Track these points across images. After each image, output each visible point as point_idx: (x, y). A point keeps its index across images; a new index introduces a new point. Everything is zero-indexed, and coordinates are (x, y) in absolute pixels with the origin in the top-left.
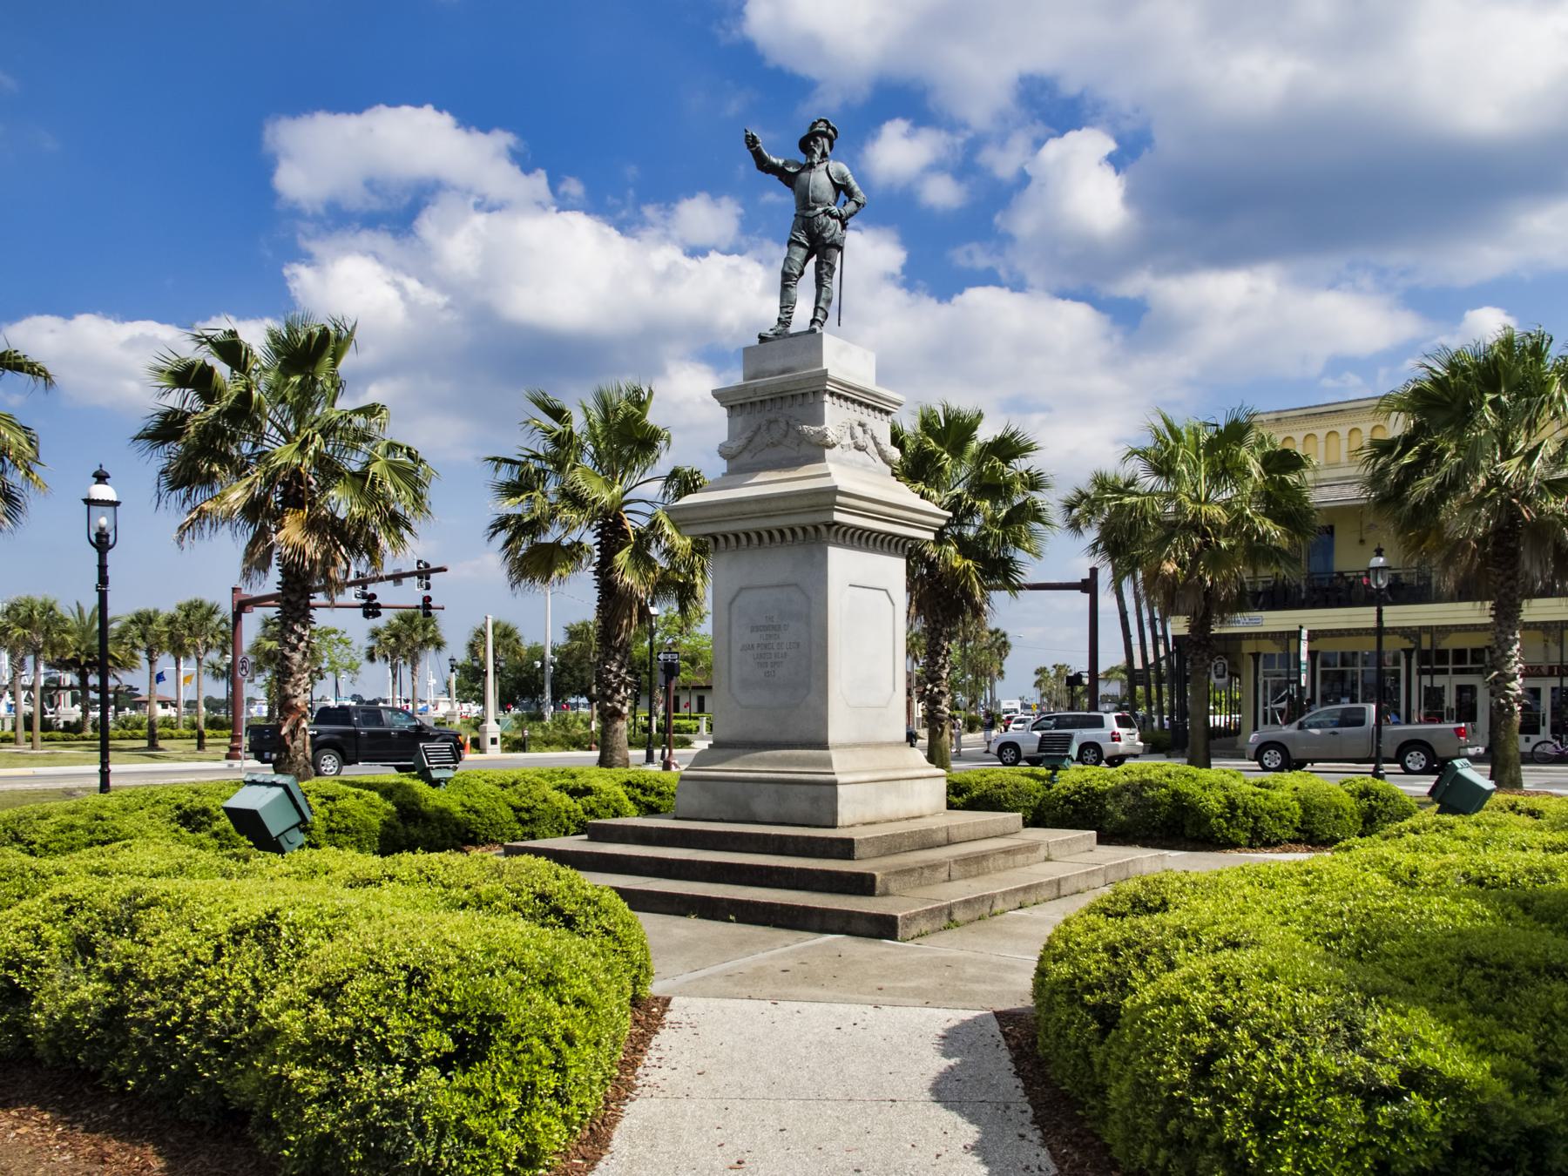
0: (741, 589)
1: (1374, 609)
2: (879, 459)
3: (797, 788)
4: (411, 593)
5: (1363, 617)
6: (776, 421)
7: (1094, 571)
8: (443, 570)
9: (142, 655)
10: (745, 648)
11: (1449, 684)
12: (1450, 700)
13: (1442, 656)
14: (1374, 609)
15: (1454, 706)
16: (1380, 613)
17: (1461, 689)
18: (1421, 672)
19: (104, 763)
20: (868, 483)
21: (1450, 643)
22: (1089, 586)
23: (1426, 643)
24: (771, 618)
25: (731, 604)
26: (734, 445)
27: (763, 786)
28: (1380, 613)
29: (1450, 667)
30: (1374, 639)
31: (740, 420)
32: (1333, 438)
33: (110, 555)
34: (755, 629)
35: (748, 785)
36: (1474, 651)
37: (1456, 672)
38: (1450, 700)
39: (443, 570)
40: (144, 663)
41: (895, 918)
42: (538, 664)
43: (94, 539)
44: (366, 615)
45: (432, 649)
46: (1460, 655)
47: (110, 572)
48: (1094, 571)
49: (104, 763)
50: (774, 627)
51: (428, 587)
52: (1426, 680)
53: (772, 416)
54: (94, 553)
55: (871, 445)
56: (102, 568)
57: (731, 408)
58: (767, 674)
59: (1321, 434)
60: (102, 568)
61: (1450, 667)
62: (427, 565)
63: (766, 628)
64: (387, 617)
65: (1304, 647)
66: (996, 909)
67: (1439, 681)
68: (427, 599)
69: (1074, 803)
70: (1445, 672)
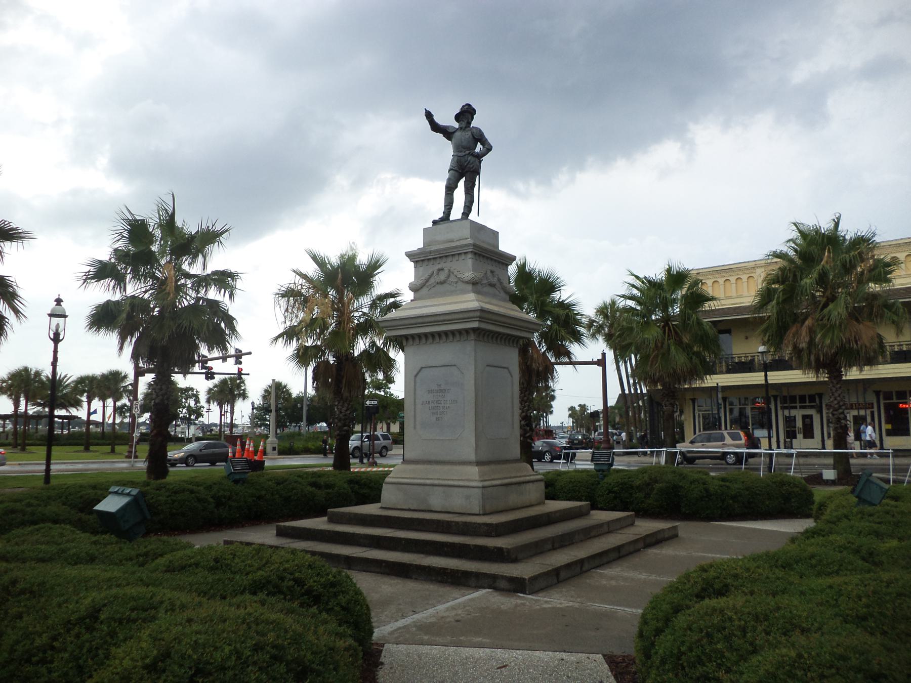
0: (422, 368)
1: (763, 374)
2: (502, 292)
3: (456, 489)
4: (230, 367)
5: (756, 378)
6: (442, 269)
7: (604, 355)
8: (250, 353)
9: (84, 399)
10: (423, 403)
11: (798, 414)
12: (799, 424)
13: (793, 399)
14: (763, 374)
15: (801, 426)
16: (766, 376)
17: (804, 417)
18: (783, 408)
19: (48, 470)
20: (450, 304)
21: (797, 392)
22: (602, 362)
23: (785, 393)
24: (440, 385)
25: (416, 376)
26: (418, 284)
27: (436, 488)
28: (766, 376)
29: (798, 405)
30: (764, 390)
31: (421, 269)
32: (716, 284)
33: (60, 345)
34: (430, 391)
35: (427, 487)
36: (810, 396)
37: (802, 407)
38: (799, 424)
39: (250, 353)
40: (85, 405)
41: (524, 579)
42: (299, 405)
43: (52, 336)
44: (207, 378)
45: (241, 399)
46: (802, 399)
47: (59, 355)
48: (604, 355)
49: (48, 470)
50: (442, 391)
51: (240, 363)
52: (786, 413)
53: (440, 266)
54: (52, 344)
55: (498, 285)
56: (55, 352)
57: (416, 262)
58: (438, 419)
59: (721, 281)
60: (55, 352)
61: (798, 405)
62: (241, 351)
63: (437, 391)
64: (218, 379)
65: (720, 396)
66: (584, 569)
67: (793, 412)
68: (240, 370)
69: (614, 492)
70: (795, 408)
